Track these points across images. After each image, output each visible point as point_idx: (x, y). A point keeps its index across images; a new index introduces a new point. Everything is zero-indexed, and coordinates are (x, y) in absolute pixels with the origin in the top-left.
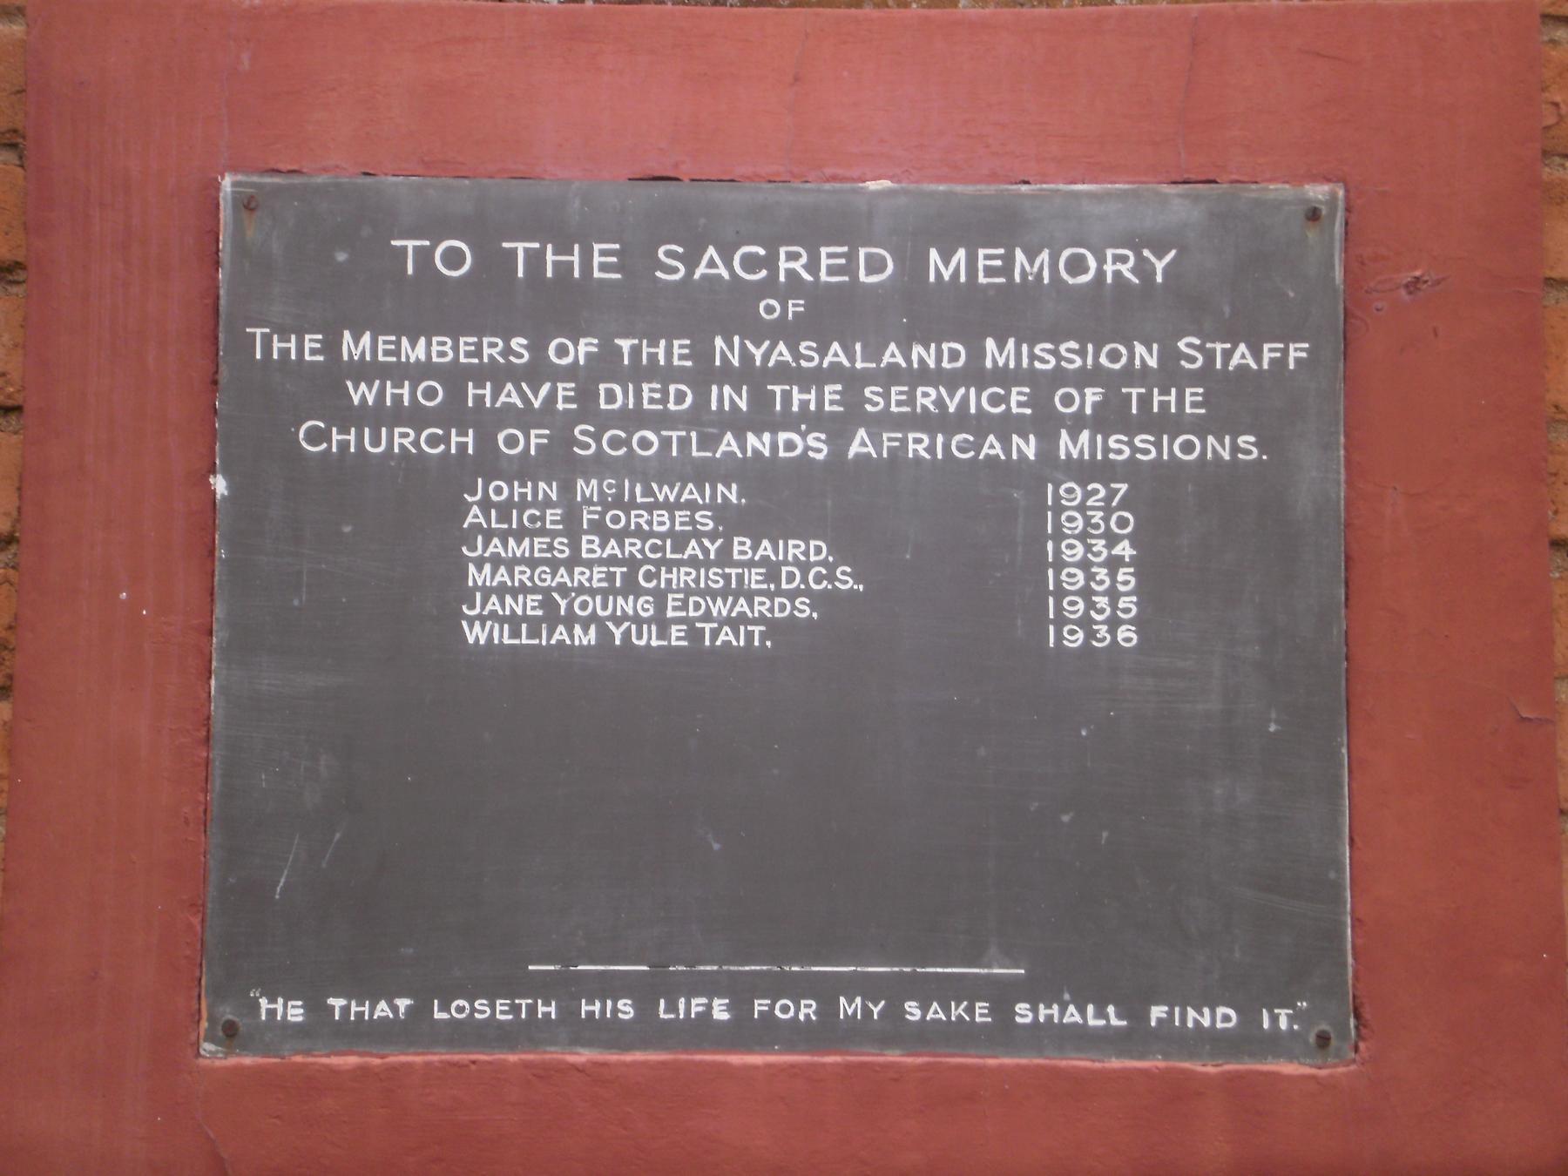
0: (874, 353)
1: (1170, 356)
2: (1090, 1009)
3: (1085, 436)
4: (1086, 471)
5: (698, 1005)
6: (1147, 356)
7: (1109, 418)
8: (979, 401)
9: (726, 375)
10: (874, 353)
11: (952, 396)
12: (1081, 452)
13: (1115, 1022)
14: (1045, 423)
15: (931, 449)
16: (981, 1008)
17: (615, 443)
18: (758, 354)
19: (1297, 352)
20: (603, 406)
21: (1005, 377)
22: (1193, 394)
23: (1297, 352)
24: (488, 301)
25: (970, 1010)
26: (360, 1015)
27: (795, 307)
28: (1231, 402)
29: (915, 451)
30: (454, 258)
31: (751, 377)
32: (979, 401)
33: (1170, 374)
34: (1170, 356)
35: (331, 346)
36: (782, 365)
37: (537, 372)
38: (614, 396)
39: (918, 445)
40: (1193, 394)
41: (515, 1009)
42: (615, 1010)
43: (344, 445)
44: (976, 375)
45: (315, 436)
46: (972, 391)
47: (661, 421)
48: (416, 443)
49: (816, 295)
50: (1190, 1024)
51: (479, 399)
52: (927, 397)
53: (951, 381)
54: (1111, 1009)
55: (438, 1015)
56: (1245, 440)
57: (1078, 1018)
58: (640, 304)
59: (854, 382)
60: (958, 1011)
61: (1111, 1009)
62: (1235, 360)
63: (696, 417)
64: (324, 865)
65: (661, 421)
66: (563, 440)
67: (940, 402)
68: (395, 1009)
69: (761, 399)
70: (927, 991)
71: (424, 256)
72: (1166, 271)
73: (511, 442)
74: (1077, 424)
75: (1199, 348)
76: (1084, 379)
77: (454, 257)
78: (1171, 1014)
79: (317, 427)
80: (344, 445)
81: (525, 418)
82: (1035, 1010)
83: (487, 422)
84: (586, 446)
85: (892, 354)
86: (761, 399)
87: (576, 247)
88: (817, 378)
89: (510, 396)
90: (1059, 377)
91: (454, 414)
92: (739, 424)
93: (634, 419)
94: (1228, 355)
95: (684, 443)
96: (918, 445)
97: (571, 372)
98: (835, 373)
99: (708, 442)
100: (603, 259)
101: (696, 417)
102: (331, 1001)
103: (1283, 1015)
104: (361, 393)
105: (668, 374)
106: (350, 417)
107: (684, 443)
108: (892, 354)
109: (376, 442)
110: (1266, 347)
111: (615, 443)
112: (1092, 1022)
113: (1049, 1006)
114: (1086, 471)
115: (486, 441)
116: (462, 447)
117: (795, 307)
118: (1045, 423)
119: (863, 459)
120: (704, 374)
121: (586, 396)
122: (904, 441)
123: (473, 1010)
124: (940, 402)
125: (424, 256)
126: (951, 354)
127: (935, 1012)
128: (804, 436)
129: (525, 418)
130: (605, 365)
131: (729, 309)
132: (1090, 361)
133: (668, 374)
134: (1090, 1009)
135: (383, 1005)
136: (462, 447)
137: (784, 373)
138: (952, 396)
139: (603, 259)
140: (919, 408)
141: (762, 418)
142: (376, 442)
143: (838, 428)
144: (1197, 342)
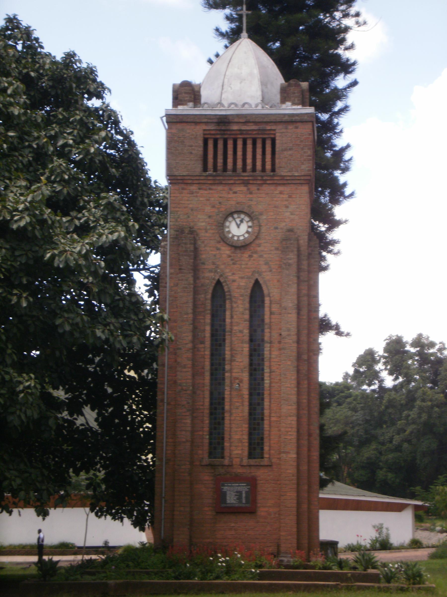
28: (248, 488)
131: (233, 486)
140: (239, 489)
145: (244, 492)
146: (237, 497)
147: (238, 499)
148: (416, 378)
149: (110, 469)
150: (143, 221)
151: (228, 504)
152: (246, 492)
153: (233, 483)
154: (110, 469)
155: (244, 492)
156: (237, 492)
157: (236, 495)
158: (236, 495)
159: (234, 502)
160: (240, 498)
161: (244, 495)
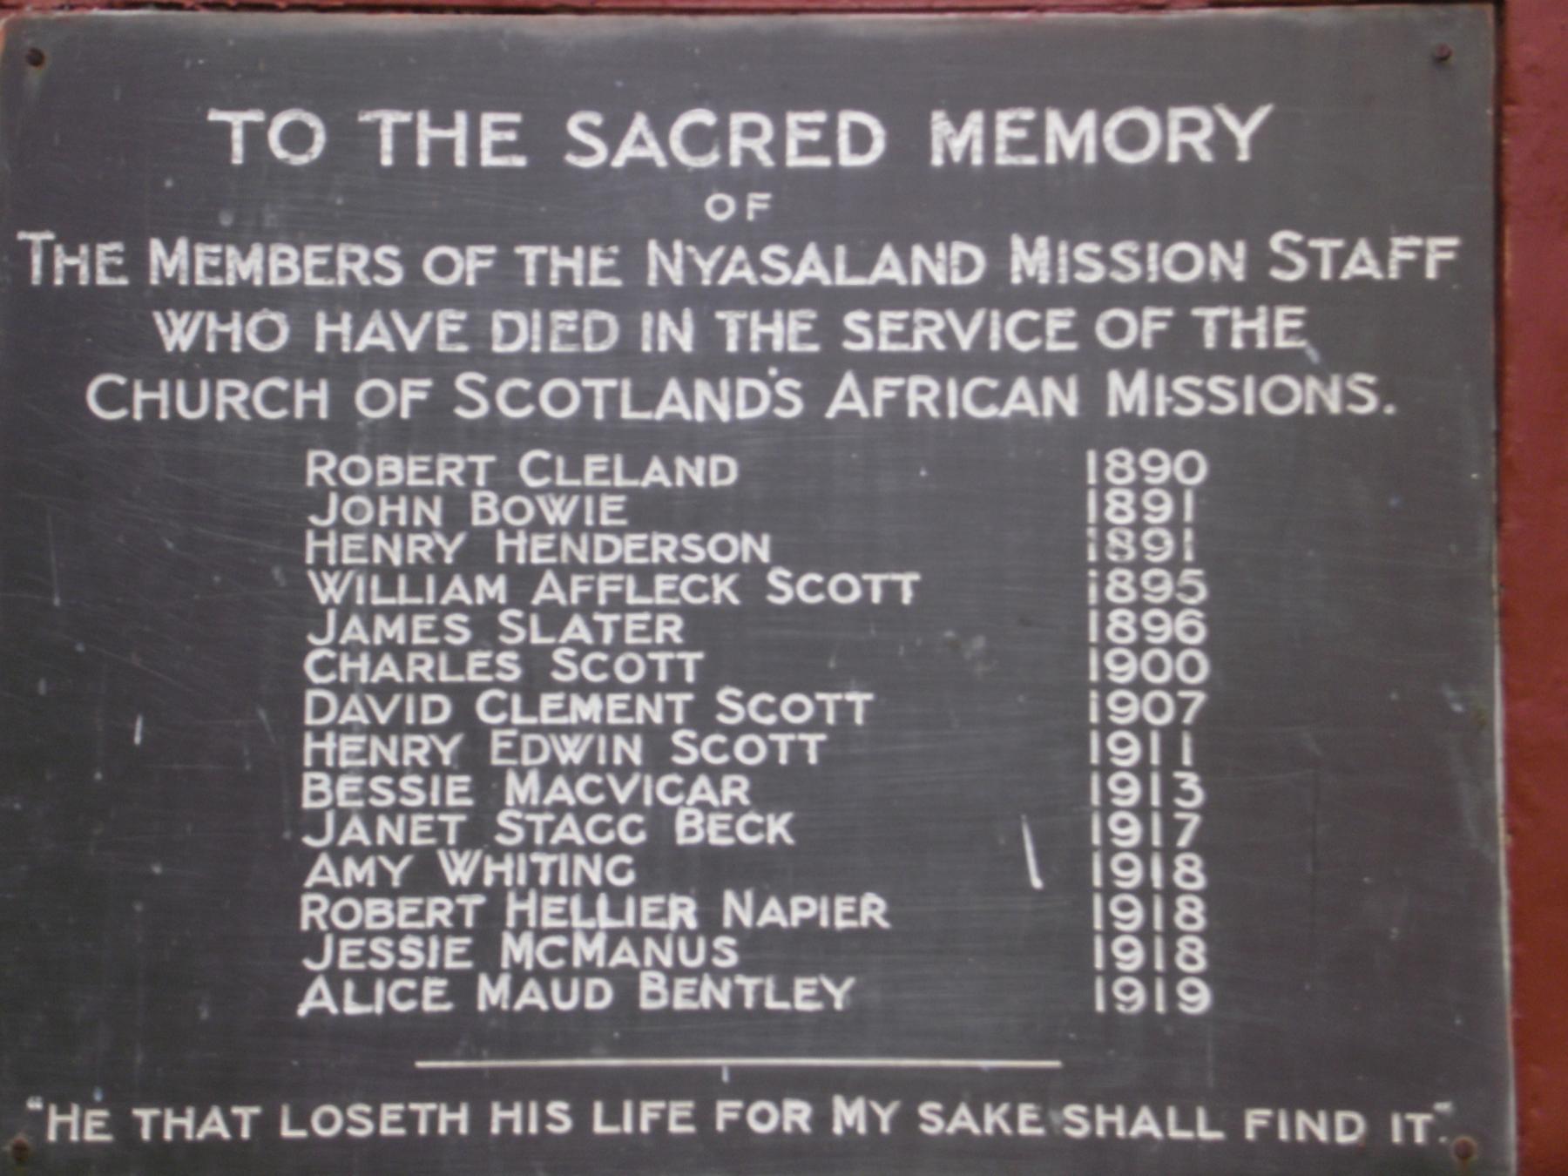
0: (860, 264)
1: (1261, 259)
2: (1172, 1114)
3: (1141, 378)
4: (1138, 432)
5: (649, 1110)
6: (1225, 260)
7: (1177, 352)
8: (1005, 331)
9: (672, 299)
10: (860, 264)
11: (965, 324)
12: (1136, 406)
13: (1205, 1134)
14: (1090, 366)
15: (941, 402)
16: (1026, 1112)
17: (516, 398)
18: (706, 266)
19: (1440, 250)
20: (497, 348)
21: (1039, 296)
22: (1287, 318)
23: (1440, 250)
24: (346, 198)
25: (1012, 1118)
26: (179, 1131)
27: (757, 202)
28: (1344, 323)
29: (921, 407)
30: (297, 137)
31: (701, 300)
32: (1005, 331)
33: (1256, 292)
34: (1261, 259)
35: (136, 262)
36: (739, 284)
37: (415, 298)
38: (518, 331)
39: (921, 393)
40: (1287, 318)
41: (409, 1120)
42: (544, 1119)
43: (152, 407)
44: (997, 292)
45: (110, 397)
46: (995, 314)
47: (579, 366)
48: (248, 404)
49: (779, 179)
50: (1301, 1136)
51: (334, 339)
52: (930, 328)
53: (961, 301)
54: (1201, 1115)
55: (287, 1132)
56: (1361, 381)
57: (1154, 1130)
58: (545, 199)
59: (829, 305)
60: (994, 1117)
61: (1201, 1115)
62: (1351, 270)
63: (625, 359)
64: (1037, 883)
65: (579, 366)
66: (443, 400)
67: (947, 335)
68: (233, 1124)
69: (710, 333)
70: (950, 1090)
71: (255, 134)
72: (1256, 139)
73: (376, 398)
74: (1129, 361)
75: (1301, 248)
76: (1139, 296)
77: (291, 135)
78: (1274, 1121)
79: (112, 385)
80: (152, 407)
81: (398, 365)
82: (1091, 1118)
83: (343, 369)
84: (472, 405)
85: (887, 268)
86: (710, 333)
87: (215, 116)
88: (788, 298)
89: (375, 336)
90: (1108, 294)
91: (300, 361)
92: (687, 369)
93: (537, 366)
94: (1340, 258)
95: (612, 397)
96: (921, 393)
97: (456, 297)
98: (809, 294)
99: (646, 398)
100: (237, 135)
101: (625, 359)
102: (137, 1112)
103: (1420, 1120)
104: (178, 332)
105: (583, 299)
106: (159, 365)
107: (612, 397)
108: (887, 268)
109: (193, 403)
110: (1398, 242)
111: (516, 398)
112: (1175, 1134)
113: (1110, 1110)
114: (1138, 432)
115: (342, 402)
116: (312, 406)
117: (757, 202)
118: (1090, 366)
119: (848, 417)
120: (630, 300)
121: (475, 332)
122: (902, 391)
123: (348, 1123)
124: (947, 335)
125: (255, 134)
126: (948, 263)
127: (963, 1118)
128: (771, 383)
129: (398, 365)
130: (502, 286)
131: (660, 203)
132: (1153, 267)
133: (583, 299)
134: (1172, 1114)
135: (215, 1114)
136: (312, 406)
137: (740, 296)
138: (965, 324)
139: (237, 135)
140: (927, 343)
141: (711, 362)
142: (193, 403)
143: (818, 375)
144: (1296, 237)
145: (1140, 505)
146: (793, 722)
147: (834, 815)
148: (1443, 266)
149: (1415, 1126)
150: (249, 128)
151: (382, 1055)
152: (1259, 490)
153: (623, 92)
154: (1415, 1126)
155: (1140, 505)
156: (798, 485)
157: (744, 645)
158: (744, 645)
159: (681, 965)
160: (938, 796)
161: (1150, 641)
